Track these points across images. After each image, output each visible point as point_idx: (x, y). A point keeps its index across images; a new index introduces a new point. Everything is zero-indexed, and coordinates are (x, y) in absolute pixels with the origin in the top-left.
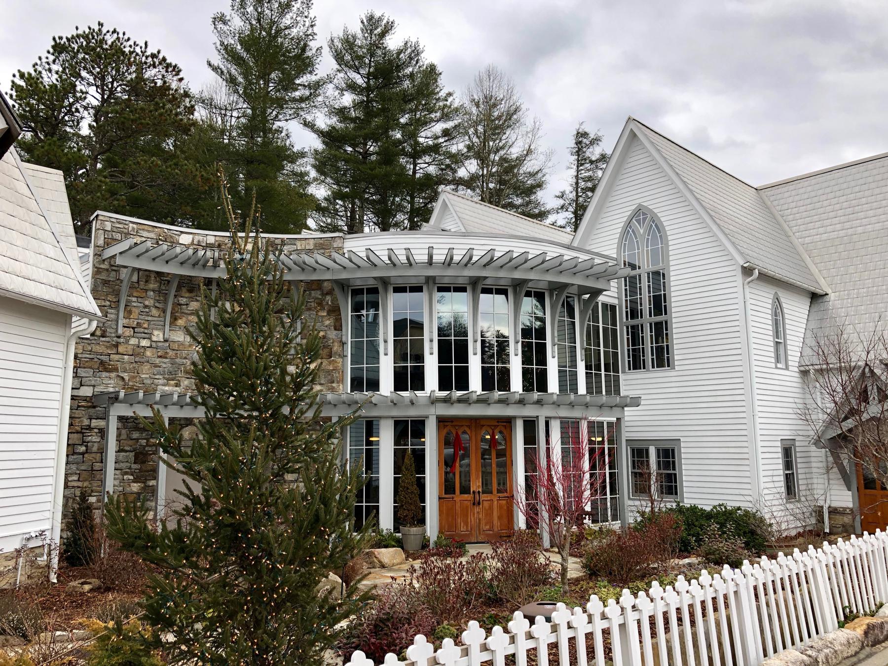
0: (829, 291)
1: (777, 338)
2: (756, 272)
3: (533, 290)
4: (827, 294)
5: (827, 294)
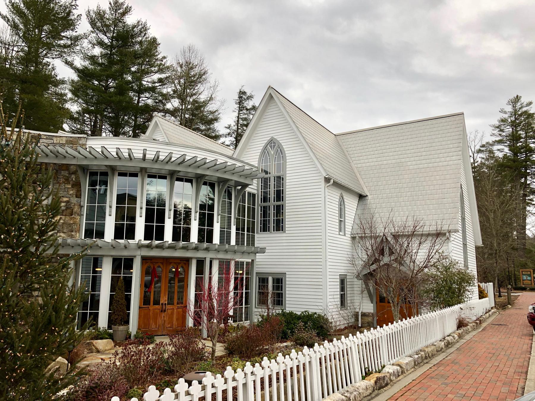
0: (368, 194)
1: (341, 218)
2: (332, 181)
3: (208, 181)
4: (367, 196)
5: (367, 196)
